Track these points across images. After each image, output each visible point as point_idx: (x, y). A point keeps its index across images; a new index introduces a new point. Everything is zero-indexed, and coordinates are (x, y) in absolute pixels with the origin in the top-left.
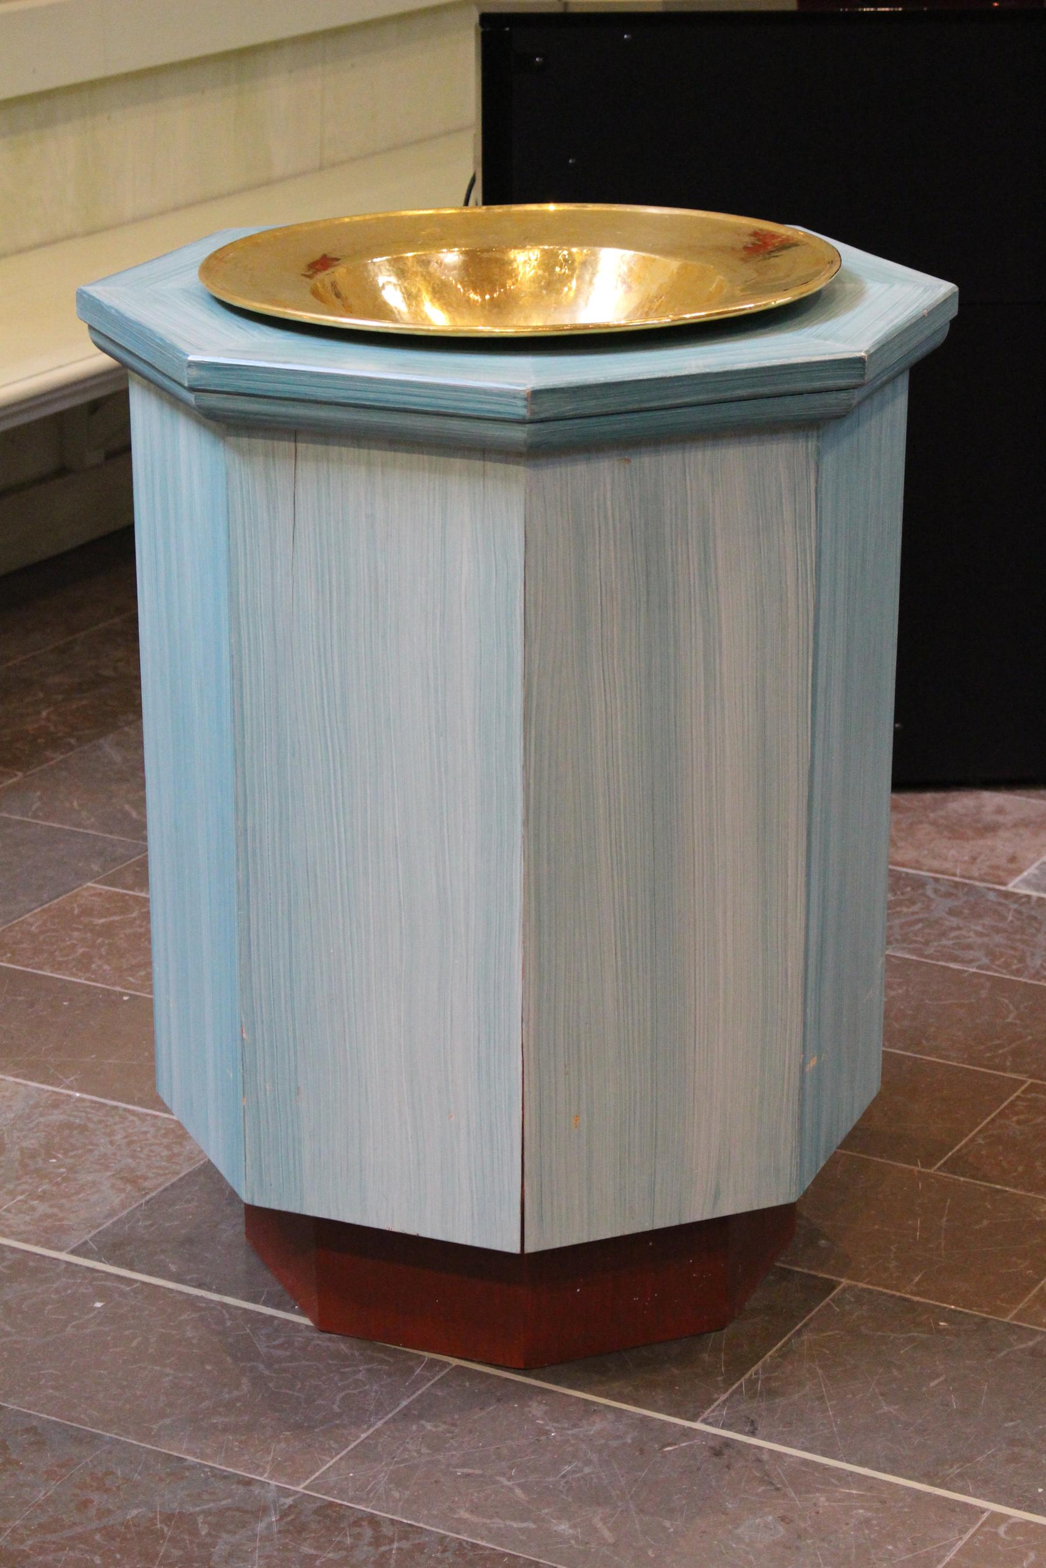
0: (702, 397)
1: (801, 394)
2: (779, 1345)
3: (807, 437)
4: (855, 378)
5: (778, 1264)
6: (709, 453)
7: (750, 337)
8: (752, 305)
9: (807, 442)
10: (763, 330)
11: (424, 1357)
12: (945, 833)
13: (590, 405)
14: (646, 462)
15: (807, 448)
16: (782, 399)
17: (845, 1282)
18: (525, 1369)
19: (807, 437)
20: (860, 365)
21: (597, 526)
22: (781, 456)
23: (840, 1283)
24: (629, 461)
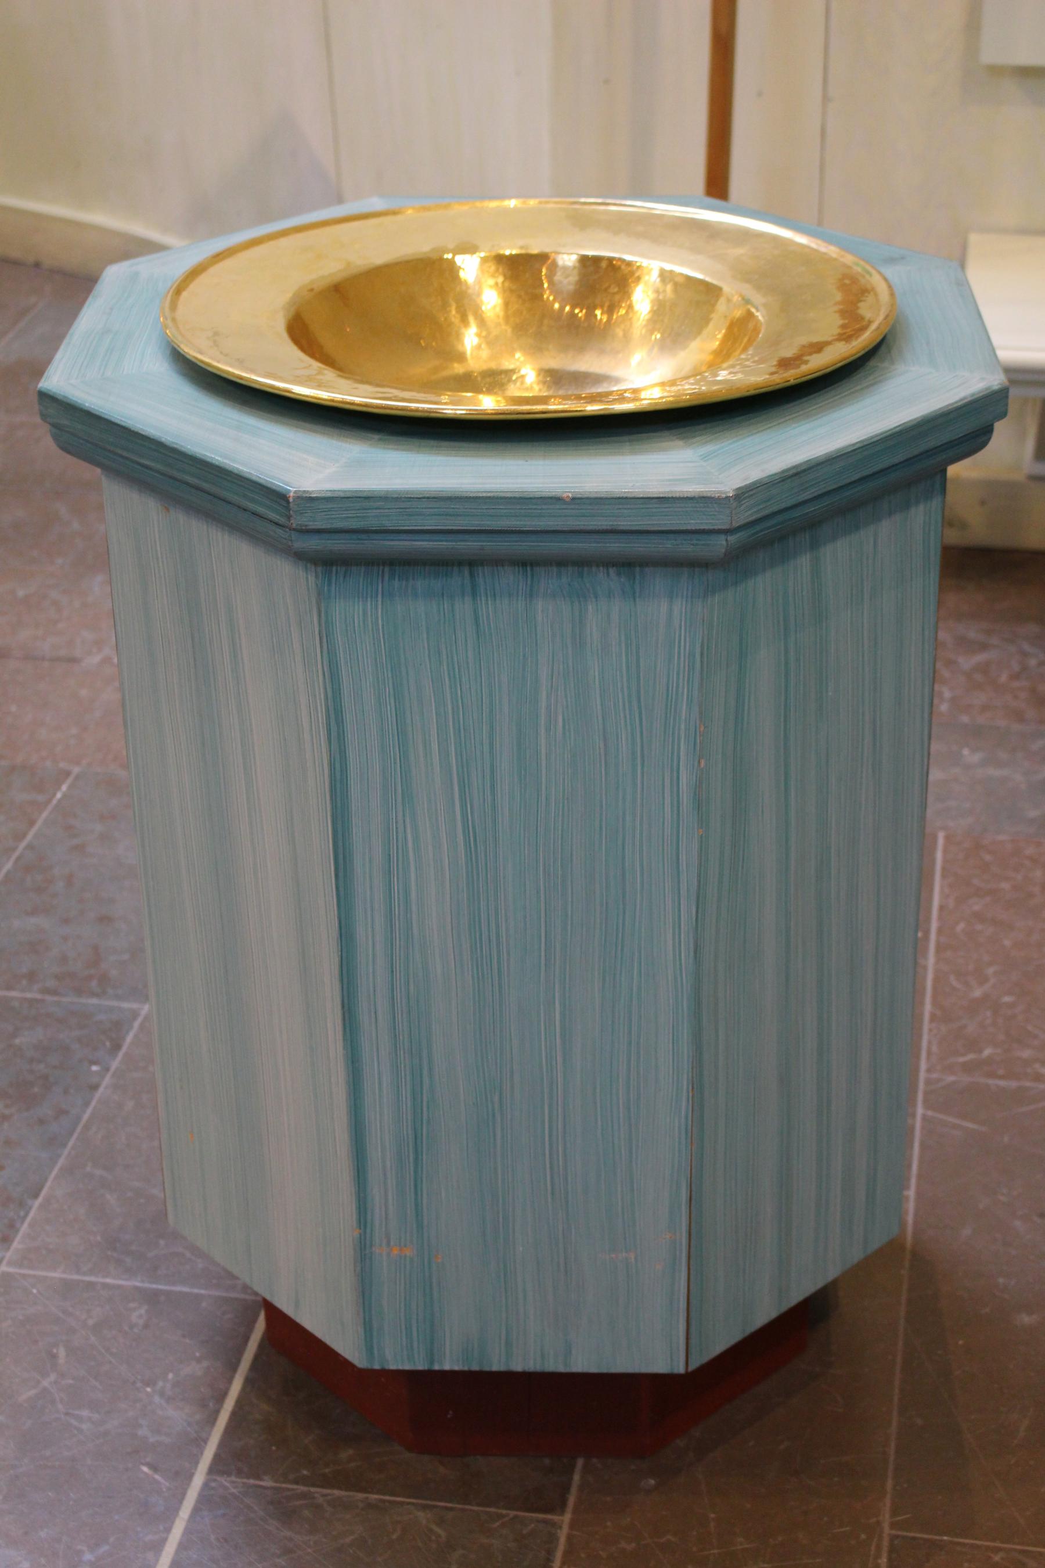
7: (310, 430)
10: (432, 442)
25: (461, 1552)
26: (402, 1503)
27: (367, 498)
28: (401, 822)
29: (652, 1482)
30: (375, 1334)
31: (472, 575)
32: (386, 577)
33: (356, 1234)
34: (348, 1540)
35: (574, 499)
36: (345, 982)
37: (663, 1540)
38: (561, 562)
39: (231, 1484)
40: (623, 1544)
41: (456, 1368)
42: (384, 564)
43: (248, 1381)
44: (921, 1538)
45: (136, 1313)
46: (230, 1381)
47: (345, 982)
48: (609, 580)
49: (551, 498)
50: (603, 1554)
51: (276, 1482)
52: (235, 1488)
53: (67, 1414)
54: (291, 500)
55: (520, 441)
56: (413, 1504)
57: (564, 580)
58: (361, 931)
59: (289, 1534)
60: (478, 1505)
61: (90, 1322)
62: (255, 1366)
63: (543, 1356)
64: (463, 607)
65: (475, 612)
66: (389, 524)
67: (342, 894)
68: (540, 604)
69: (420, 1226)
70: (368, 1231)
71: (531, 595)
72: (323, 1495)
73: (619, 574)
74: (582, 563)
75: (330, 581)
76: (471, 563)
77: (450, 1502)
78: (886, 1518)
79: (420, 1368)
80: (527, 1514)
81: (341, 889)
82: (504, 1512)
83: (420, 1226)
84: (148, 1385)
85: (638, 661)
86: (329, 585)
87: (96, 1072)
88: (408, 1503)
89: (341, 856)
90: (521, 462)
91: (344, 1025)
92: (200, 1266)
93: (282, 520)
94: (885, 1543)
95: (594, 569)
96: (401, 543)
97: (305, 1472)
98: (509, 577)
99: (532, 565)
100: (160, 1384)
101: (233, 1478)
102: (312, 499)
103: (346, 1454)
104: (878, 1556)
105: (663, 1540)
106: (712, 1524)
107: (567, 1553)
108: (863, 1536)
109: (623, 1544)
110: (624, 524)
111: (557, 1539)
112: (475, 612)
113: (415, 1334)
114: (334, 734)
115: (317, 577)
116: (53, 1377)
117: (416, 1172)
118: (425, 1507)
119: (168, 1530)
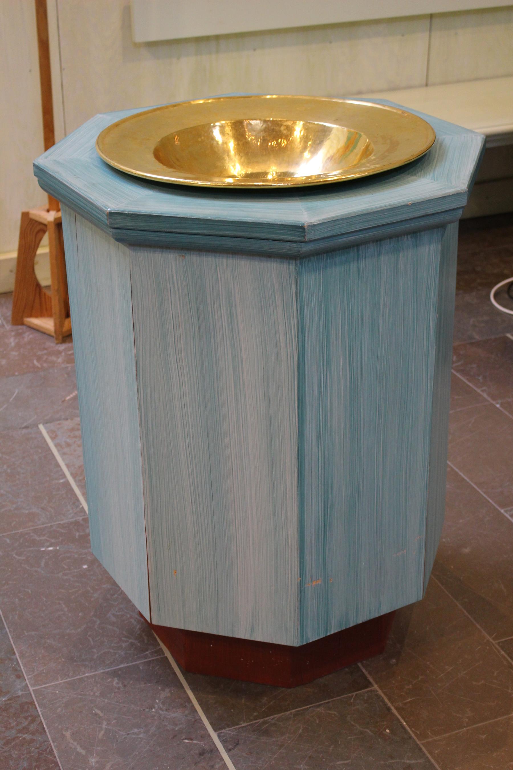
0: (206, 232)
1: (268, 240)
2: (304, 708)
3: (289, 263)
4: (299, 237)
5: (360, 665)
6: (230, 261)
7: (250, 201)
8: (282, 184)
9: (289, 265)
10: (323, 196)
11: (159, 645)
12: (66, 525)
13: (142, 225)
14: (194, 259)
15: (289, 269)
16: (256, 241)
17: (376, 687)
18: (187, 670)
19: (289, 263)
20: (301, 230)
21: (169, 287)
22: (274, 271)
23: (372, 686)
24: (184, 257)
25: (349, 716)
26: (307, 709)
27: (335, 220)
28: (325, 374)
29: (394, 660)
30: (304, 626)
31: (358, 251)
32: (325, 259)
33: (299, 581)
34: (301, 731)
35: (412, 204)
36: (300, 458)
37: (420, 679)
38: (390, 237)
39: (229, 731)
40: (407, 687)
41: (336, 631)
42: (324, 253)
43: (193, 690)
44: (509, 640)
45: (115, 683)
46: (185, 692)
47: (300, 458)
48: (407, 241)
49: (404, 205)
50: (403, 693)
51: (246, 723)
52: (232, 732)
53: (128, 734)
54: (306, 228)
55: (261, 199)
56: (312, 707)
57: (392, 245)
58: (307, 432)
59: (274, 739)
60: (338, 696)
61: (97, 694)
62: (189, 684)
63: (370, 612)
64: (354, 266)
65: (358, 268)
66: (343, 231)
67: (300, 416)
68: (382, 258)
69: (324, 566)
70: (304, 578)
71: (380, 254)
72: (272, 719)
73: (411, 237)
74: (397, 236)
75: (302, 266)
76: (356, 245)
77: (326, 700)
78: (488, 637)
79: (322, 637)
80: (359, 692)
81: (300, 413)
82: (350, 695)
83: (324, 566)
84: (152, 709)
85: (417, 275)
86: (302, 269)
87: (85, 564)
88: (310, 707)
89: (301, 398)
90: (371, 195)
91: (298, 479)
92: (122, 653)
93: (302, 239)
94: (497, 646)
95: (403, 237)
96: (345, 239)
97: (255, 714)
98: (372, 248)
99: (380, 241)
100: (156, 706)
101: (227, 729)
102: (314, 226)
103: (265, 700)
104: (499, 652)
105: (420, 679)
106: (431, 666)
107: (390, 699)
108: (488, 648)
109: (407, 687)
110: (430, 211)
111: (380, 695)
112: (358, 268)
113: (320, 621)
114: (300, 339)
115: (296, 265)
116: (105, 723)
117: (324, 542)
118: (318, 706)
119: (222, 759)
